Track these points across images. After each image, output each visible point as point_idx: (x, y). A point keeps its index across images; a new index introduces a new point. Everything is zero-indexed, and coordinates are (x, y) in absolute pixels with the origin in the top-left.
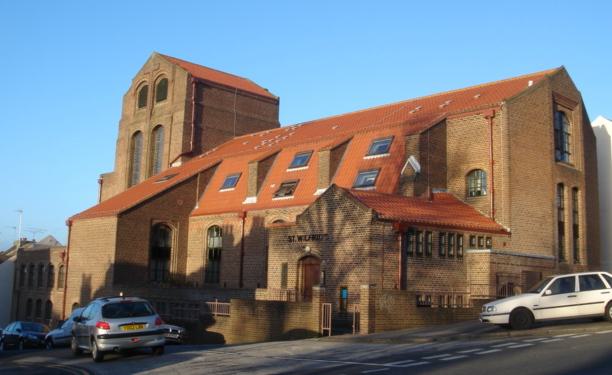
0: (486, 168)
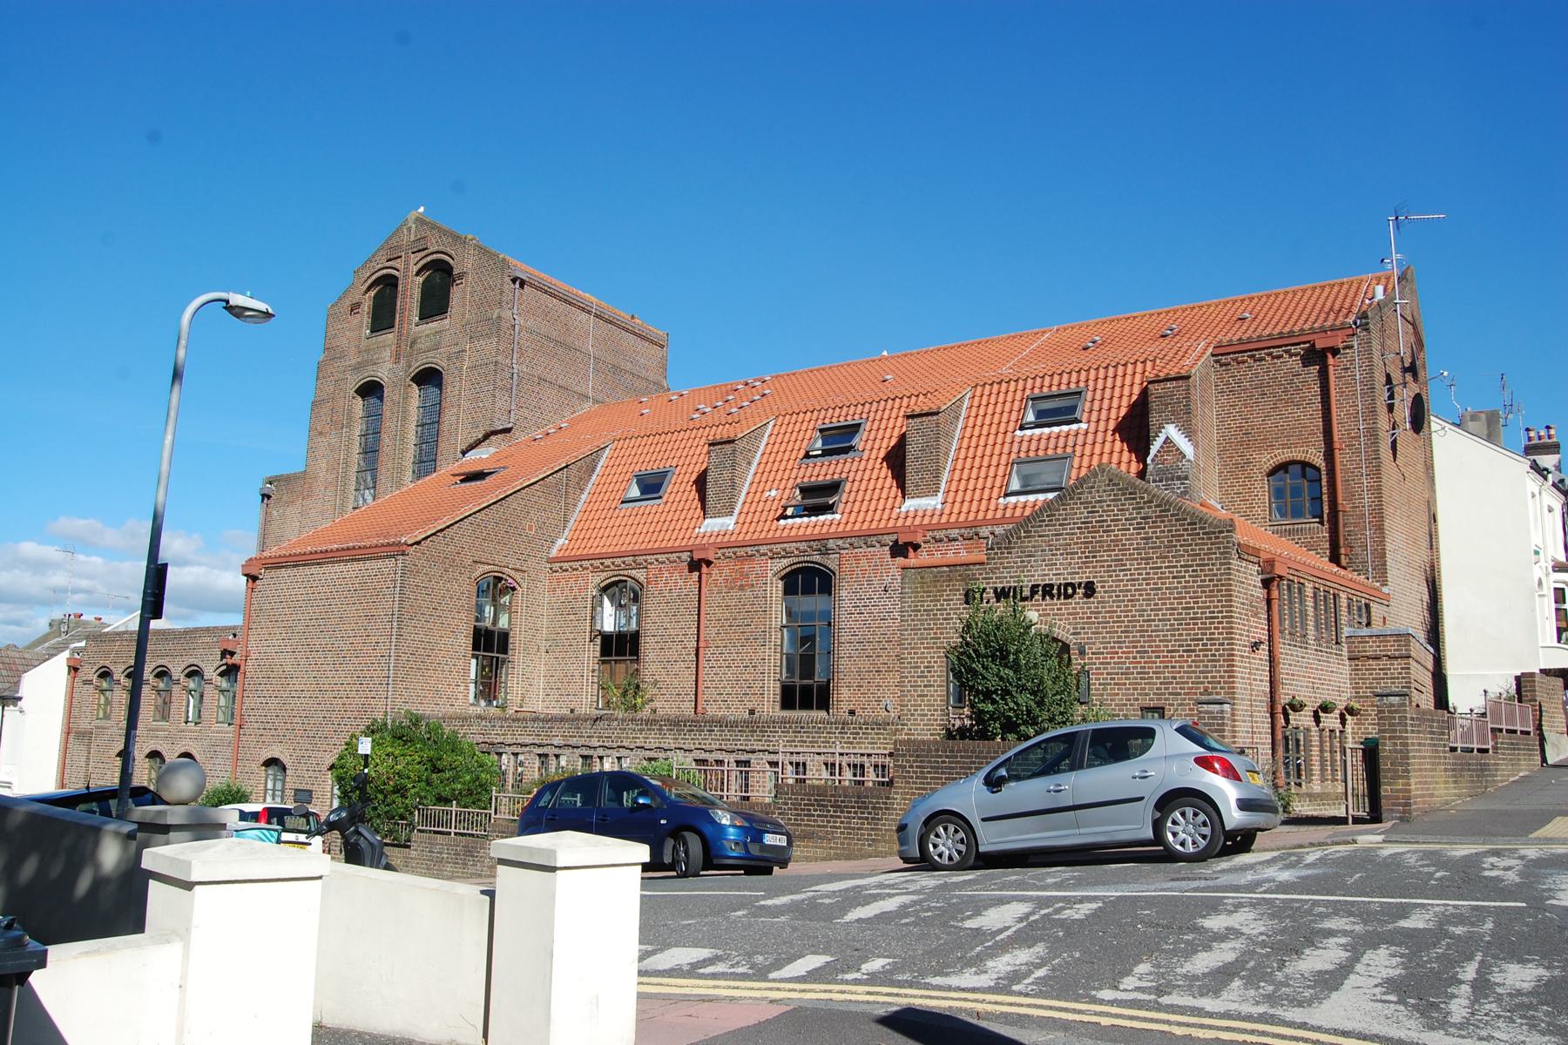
0: (1319, 461)
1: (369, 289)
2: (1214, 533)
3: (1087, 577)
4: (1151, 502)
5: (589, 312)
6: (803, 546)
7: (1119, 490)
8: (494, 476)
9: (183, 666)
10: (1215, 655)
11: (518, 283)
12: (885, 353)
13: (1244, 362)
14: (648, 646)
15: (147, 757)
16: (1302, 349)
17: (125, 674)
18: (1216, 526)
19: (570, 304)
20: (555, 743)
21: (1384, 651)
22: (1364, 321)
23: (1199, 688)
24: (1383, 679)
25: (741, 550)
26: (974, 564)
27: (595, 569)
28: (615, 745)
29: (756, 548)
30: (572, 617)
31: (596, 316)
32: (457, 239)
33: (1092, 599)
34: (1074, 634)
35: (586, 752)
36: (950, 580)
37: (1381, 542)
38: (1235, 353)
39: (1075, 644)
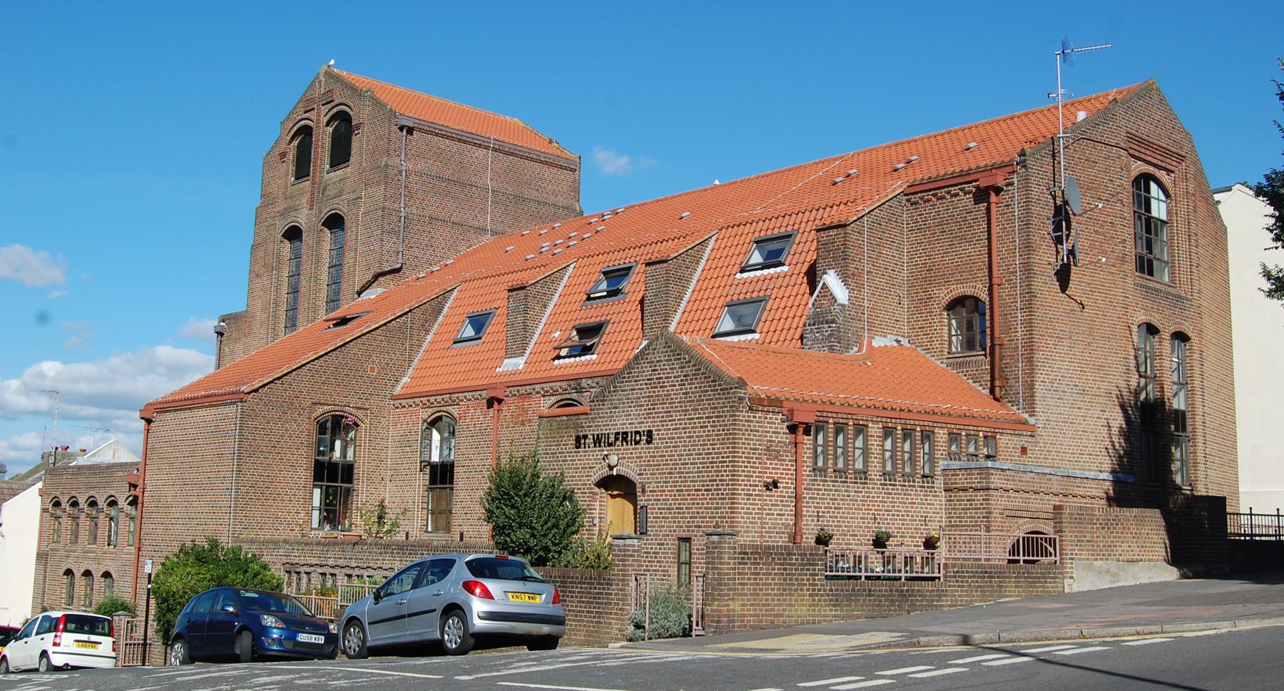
0: (984, 296)
1: (292, 139)
2: (727, 389)
3: (649, 427)
4: (690, 362)
5: (487, 148)
6: (564, 385)
7: (671, 351)
8: (355, 322)
9: (105, 497)
10: (722, 494)
11: (405, 131)
12: (717, 182)
13: (929, 201)
14: (459, 472)
15: (83, 575)
16: (974, 187)
17: (88, 503)
18: (729, 384)
19: (465, 142)
20: (330, 563)
21: (970, 483)
22: (1022, 158)
23: (713, 522)
24: (969, 509)
25: (523, 387)
26: (582, 414)
27: (425, 406)
28: (365, 566)
29: (533, 387)
30: (408, 449)
31: (495, 150)
32: (354, 91)
33: (651, 445)
34: (640, 474)
35: (349, 572)
36: (567, 428)
37: (1030, 373)
38: (921, 192)
39: (640, 483)
